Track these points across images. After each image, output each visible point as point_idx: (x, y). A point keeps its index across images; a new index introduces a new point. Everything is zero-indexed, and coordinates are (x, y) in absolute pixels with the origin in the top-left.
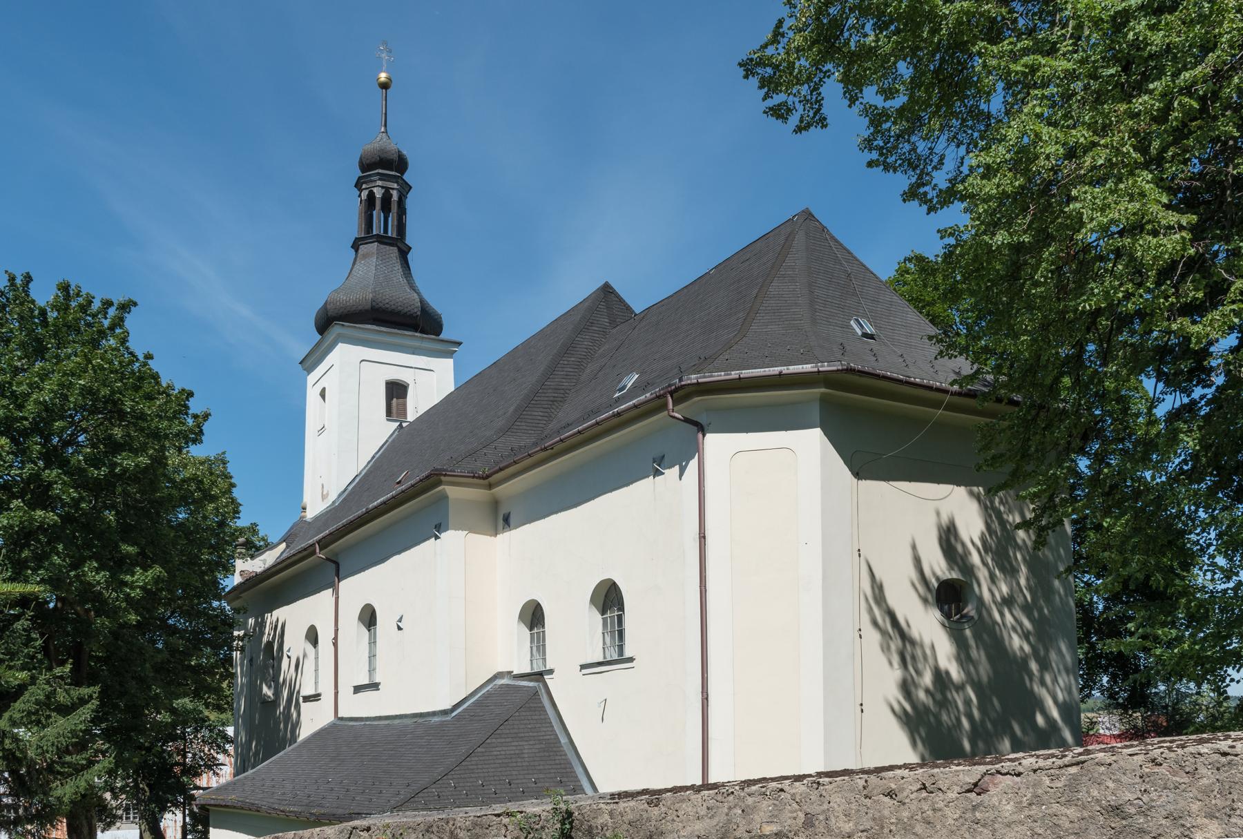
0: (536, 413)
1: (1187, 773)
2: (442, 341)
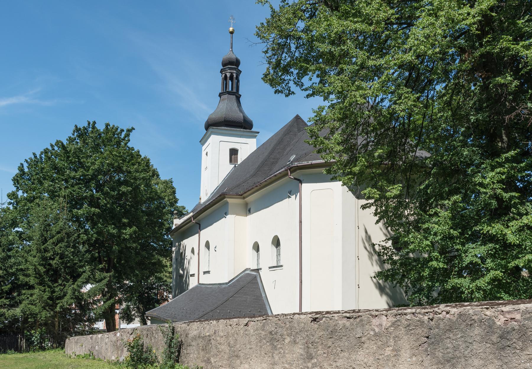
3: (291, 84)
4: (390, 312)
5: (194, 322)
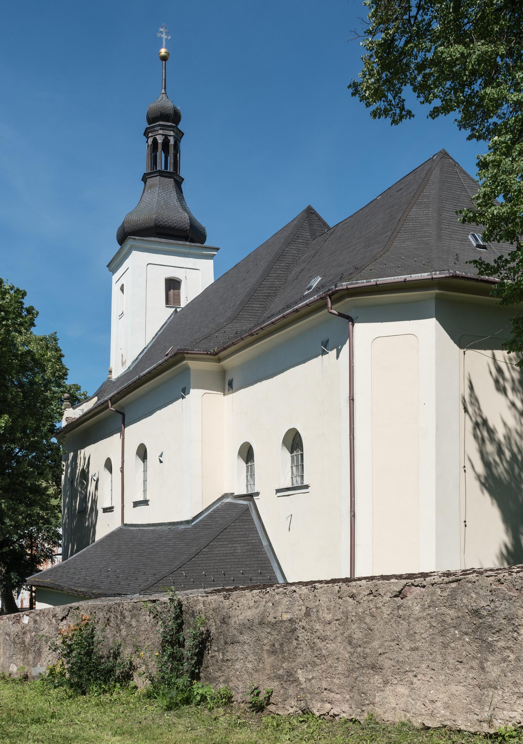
0: (255, 306)
1: (517, 590)
2: (205, 247)
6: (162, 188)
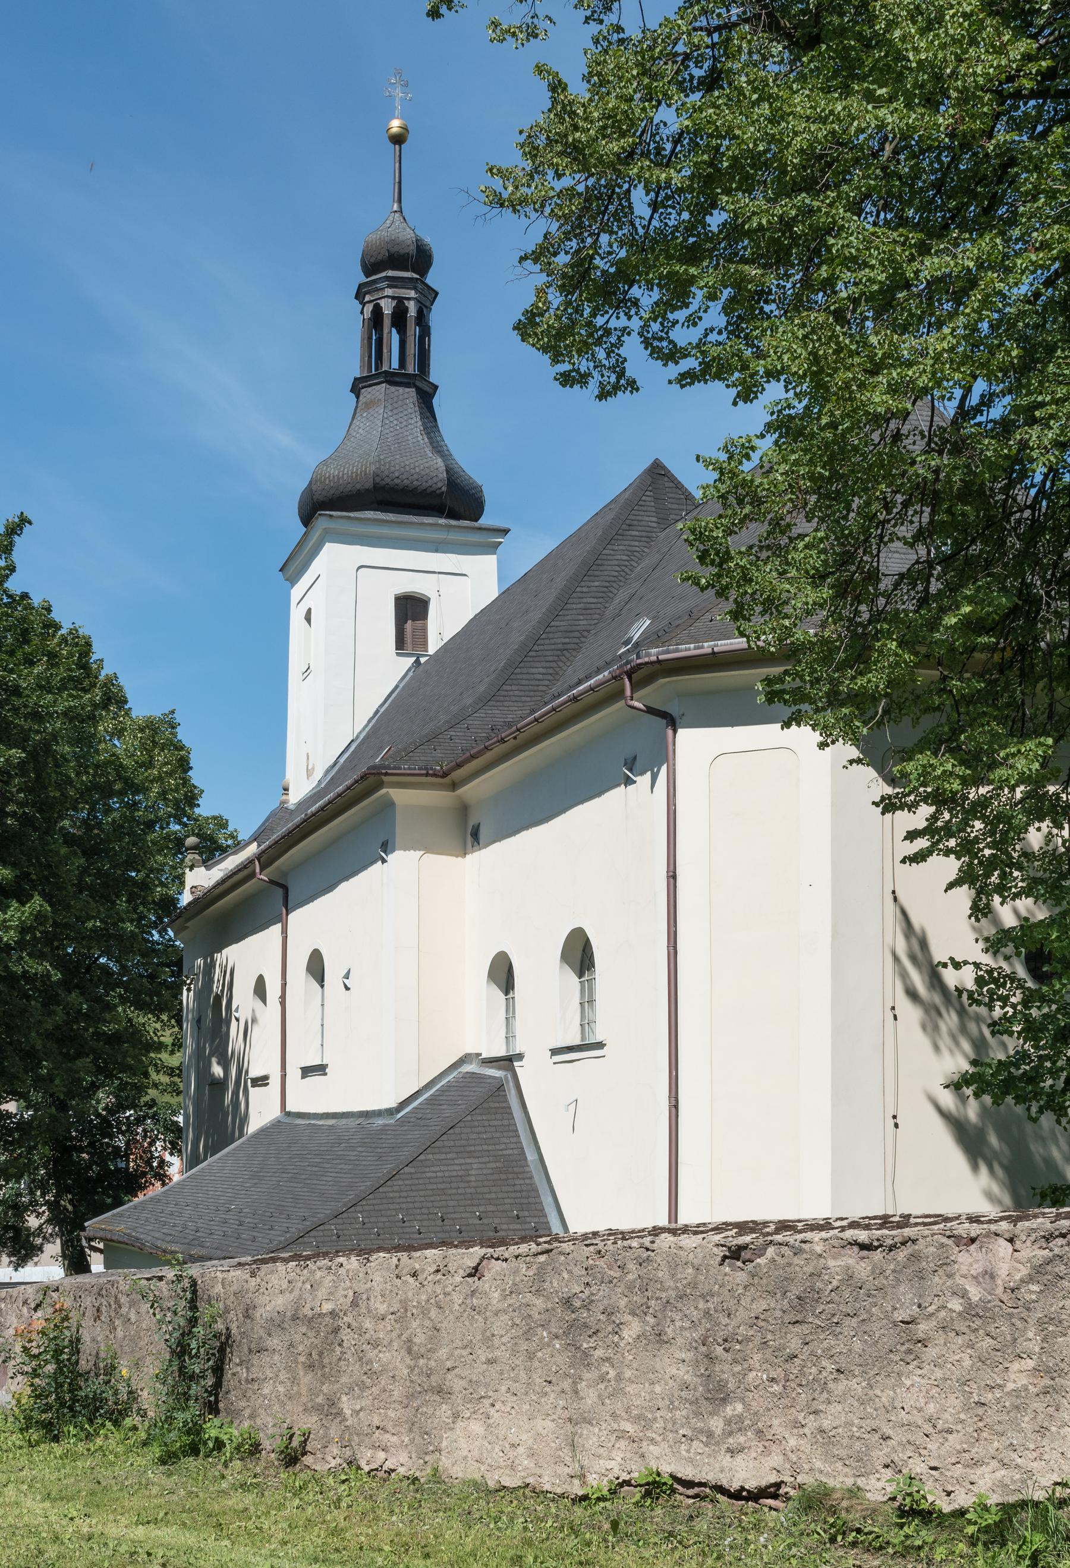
2: (480, 529)
3: (633, 349)
4: (1027, 1224)
5: (274, 1260)
6: (390, 407)
